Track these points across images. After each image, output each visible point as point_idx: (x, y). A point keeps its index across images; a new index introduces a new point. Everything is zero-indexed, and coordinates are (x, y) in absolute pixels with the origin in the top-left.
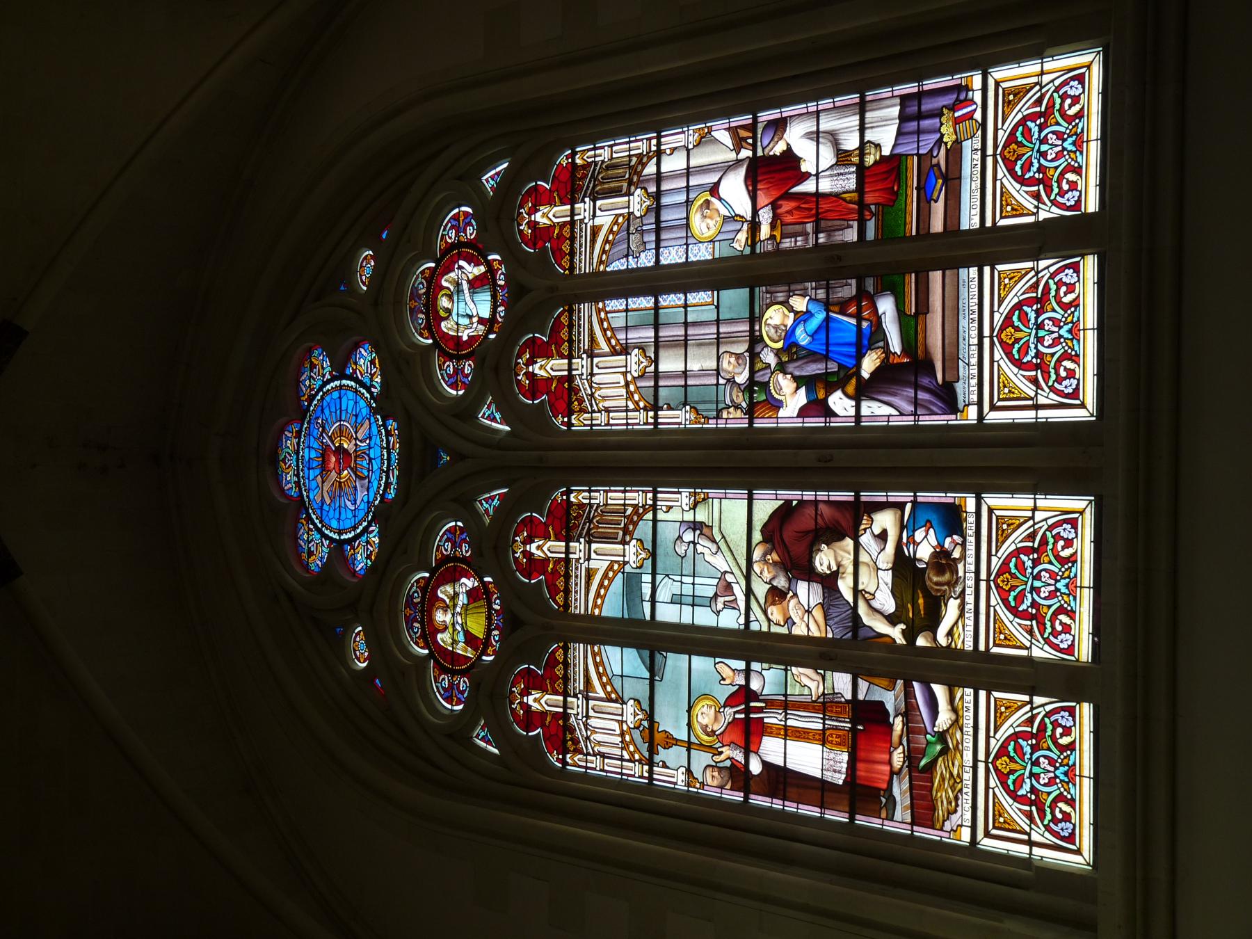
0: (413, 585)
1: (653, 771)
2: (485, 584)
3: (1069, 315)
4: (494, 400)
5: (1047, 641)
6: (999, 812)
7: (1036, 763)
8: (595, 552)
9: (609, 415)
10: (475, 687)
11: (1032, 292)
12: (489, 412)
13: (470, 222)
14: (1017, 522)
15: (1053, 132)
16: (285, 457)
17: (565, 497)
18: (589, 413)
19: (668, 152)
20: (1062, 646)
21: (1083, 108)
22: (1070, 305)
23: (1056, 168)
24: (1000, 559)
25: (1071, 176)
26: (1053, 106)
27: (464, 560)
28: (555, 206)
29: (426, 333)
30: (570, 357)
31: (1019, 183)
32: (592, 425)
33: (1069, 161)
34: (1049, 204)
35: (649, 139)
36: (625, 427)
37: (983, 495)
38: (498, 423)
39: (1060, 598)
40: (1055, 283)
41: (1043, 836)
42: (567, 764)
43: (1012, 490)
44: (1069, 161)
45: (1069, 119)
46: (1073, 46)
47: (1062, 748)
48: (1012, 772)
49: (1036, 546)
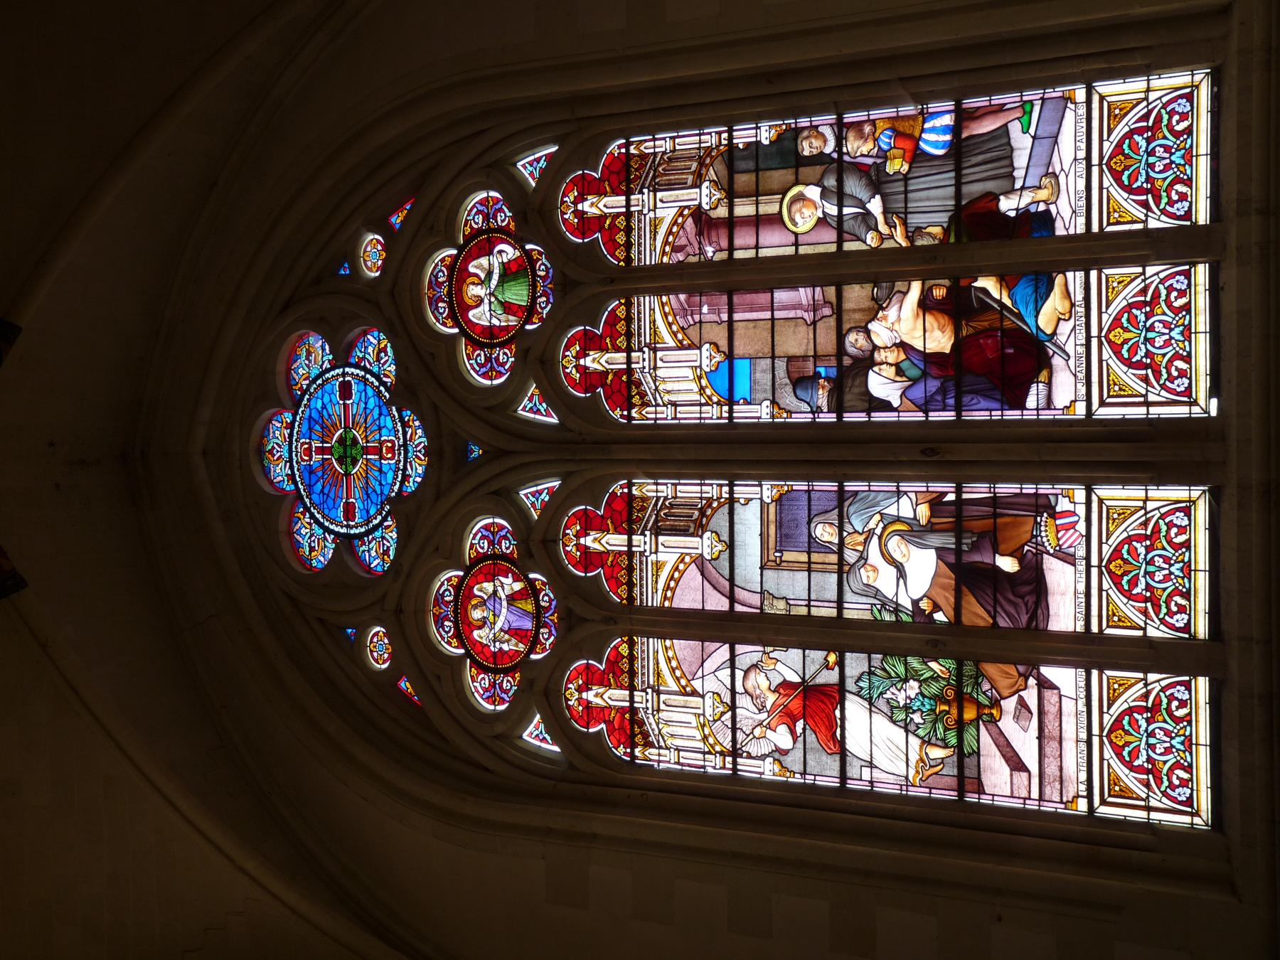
0: (442, 584)
1: (736, 762)
2: (528, 253)
3: (1180, 318)
4: (544, 720)
5: (1163, 621)
6: (1115, 780)
7: (1151, 562)
8: (664, 703)
9: (676, 410)
10: (522, 356)
11: (1142, 701)
12: (531, 405)
13: (501, 208)
14: (1129, 683)
15: (1160, 321)
16: (273, 448)
17: (623, 150)
18: (653, 406)
19: (742, 501)
20: (1179, 390)
21: (1191, 125)
22: (1182, 545)
23: (1165, 179)
24: (1111, 546)
25: (1180, 188)
26: (1159, 296)
27: (504, 557)
28: (607, 352)
29: (449, 322)
30: (629, 350)
31: (1126, 366)
32: (656, 419)
33: (1174, 558)
34: (1159, 388)
35: (719, 133)
36: (698, 421)
37: (1094, 84)
38: (543, 415)
39: (1176, 754)
40: (1165, 524)
41: (1160, 801)
42: (636, 758)
43: (1124, 482)
44: (1178, 173)
45: (1177, 135)
46: (1177, 832)
47: (1176, 547)
48: (1126, 341)
49: (1150, 705)
